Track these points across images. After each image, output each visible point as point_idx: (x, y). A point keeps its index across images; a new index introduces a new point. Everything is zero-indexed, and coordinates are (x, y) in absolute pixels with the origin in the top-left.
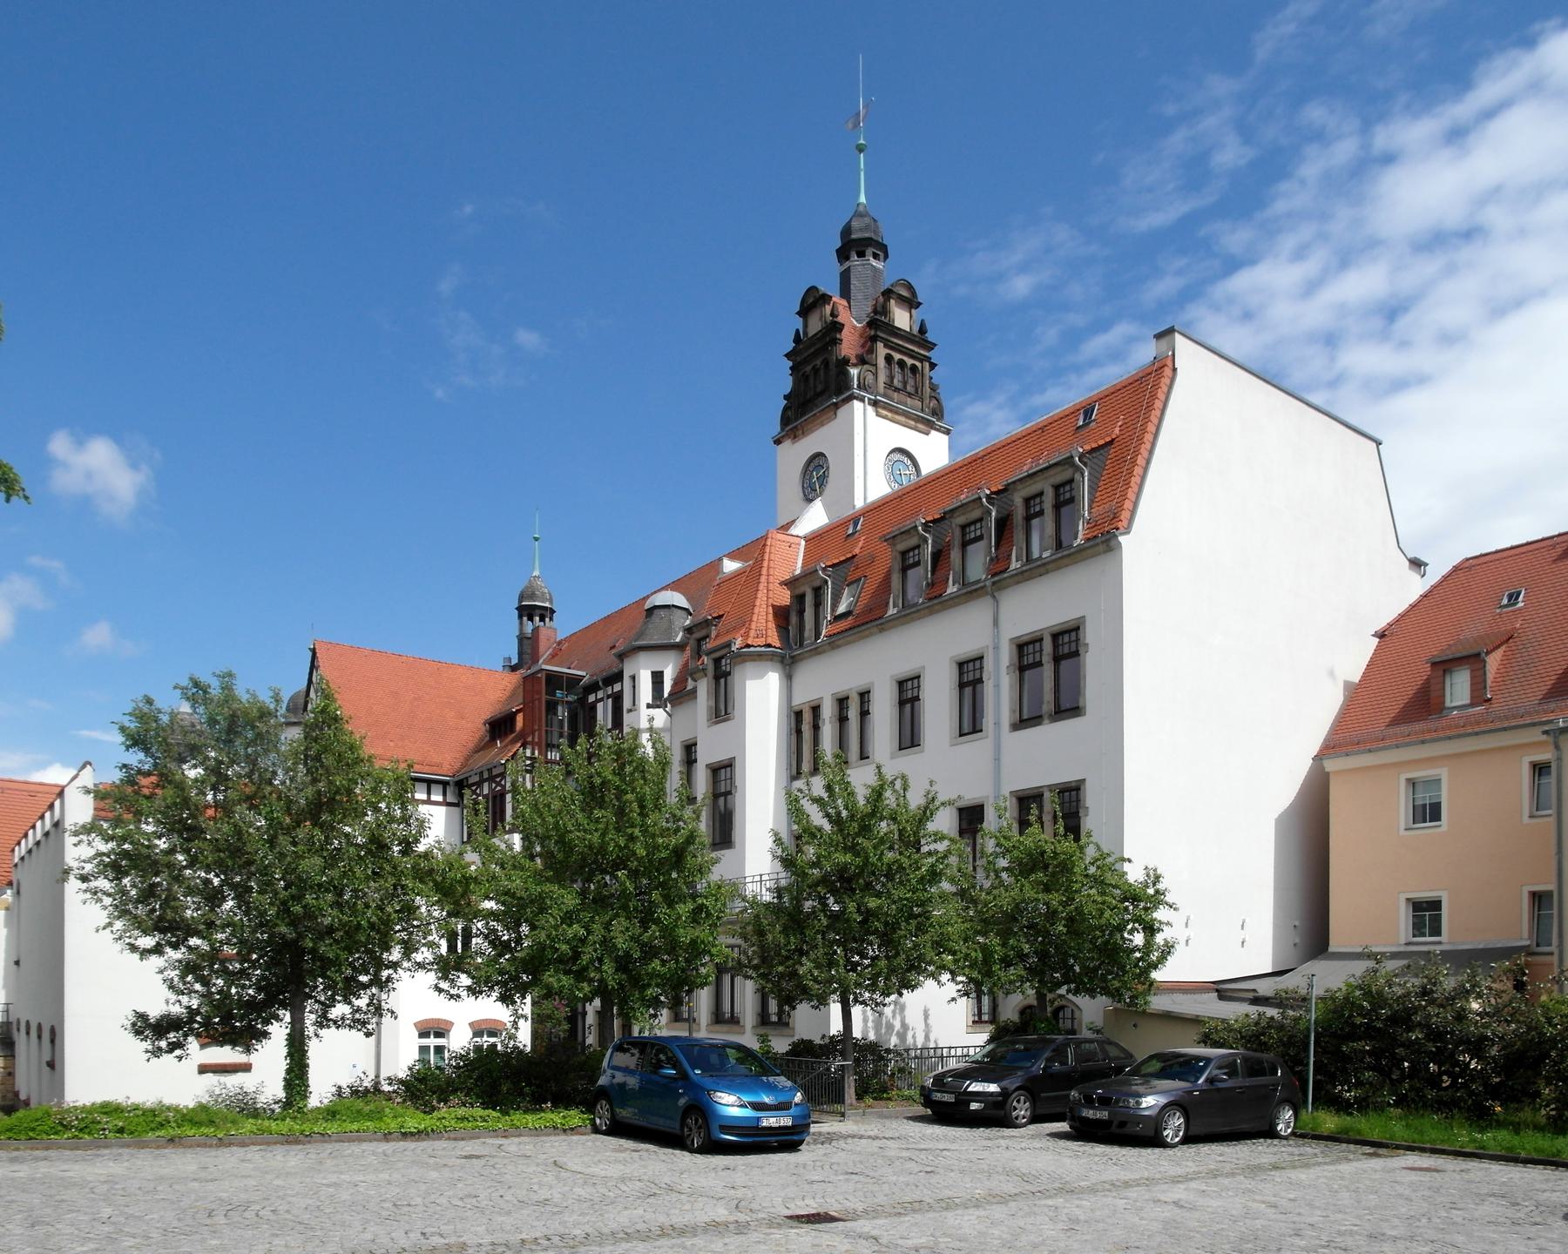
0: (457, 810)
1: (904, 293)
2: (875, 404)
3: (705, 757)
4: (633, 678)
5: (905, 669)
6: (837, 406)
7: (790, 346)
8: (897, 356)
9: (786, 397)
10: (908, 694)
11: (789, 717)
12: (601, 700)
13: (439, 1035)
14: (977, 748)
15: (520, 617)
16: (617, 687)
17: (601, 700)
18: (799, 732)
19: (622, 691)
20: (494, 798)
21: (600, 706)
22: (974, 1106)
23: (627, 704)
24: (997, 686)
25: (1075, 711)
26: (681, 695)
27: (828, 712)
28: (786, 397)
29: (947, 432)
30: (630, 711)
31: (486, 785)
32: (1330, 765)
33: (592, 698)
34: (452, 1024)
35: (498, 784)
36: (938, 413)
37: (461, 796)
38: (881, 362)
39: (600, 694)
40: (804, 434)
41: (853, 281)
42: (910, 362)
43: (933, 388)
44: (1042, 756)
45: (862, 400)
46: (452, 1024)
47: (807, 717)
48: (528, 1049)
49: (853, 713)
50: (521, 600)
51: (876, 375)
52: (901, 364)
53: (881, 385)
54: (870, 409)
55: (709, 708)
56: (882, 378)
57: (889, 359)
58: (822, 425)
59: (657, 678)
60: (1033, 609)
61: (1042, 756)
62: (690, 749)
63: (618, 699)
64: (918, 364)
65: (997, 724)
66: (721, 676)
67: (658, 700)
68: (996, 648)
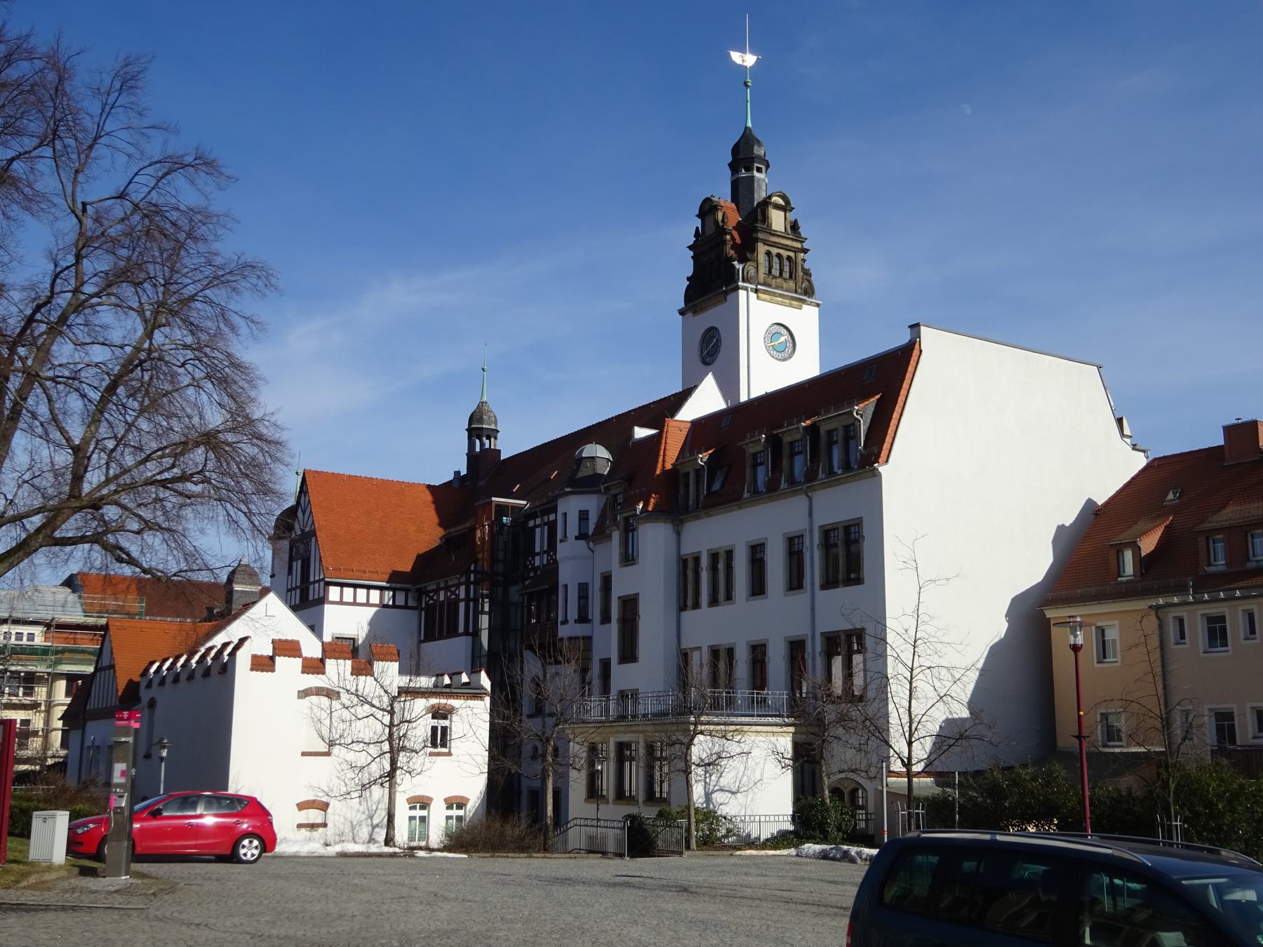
0: (416, 613)
1: (781, 202)
2: (756, 291)
3: (618, 591)
4: (565, 514)
5: (755, 537)
6: (726, 293)
7: (692, 240)
8: (775, 251)
9: (688, 279)
10: (757, 554)
11: (678, 562)
12: (539, 526)
13: (423, 808)
14: (801, 598)
15: (470, 437)
16: (552, 517)
17: (539, 526)
18: (685, 575)
19: (555, 521)
20: (449, 604)
21: (538, 531)
22: (968, 865)
23: (559, 535)
24: (812, 558)
25: (859, 581)
26: (601, 534)
27: (704, 562)
28: (688, 279)
29: (818, 305)
30: (562, 541)
31: (442, 593)
32: (1050, 613)
33: (531, 523)
34: (431, 799)
35: (453, 593)
36: (809, 291)
37: (420, 600)
38: (762, 258)
39: (538, 521)
40: (702, 310)
41: (741, 188)
42: (785, 253)
43: (807, 273)
44: (834, 611)
45: (746, 289)
46: (431, 799)
47: (691, 565)
48: (360, 642)
49: (721, 566)
50: (470, 424)
51: (757, 268)
52: (779, 256)
53: (762, 276)
54: (753, 295)
55: (621, 554)
56: (763, 269)
57: (768, 254)
58: (715, 305)
59: (583, 516)
60: (832, 505)
61: (834, 611)
62: (607, 580)
63: (552, 526)
64: (792, 254)
65: (812, 584)
66: (629, 530)
67: (582, 536)
68: (811, 531)
